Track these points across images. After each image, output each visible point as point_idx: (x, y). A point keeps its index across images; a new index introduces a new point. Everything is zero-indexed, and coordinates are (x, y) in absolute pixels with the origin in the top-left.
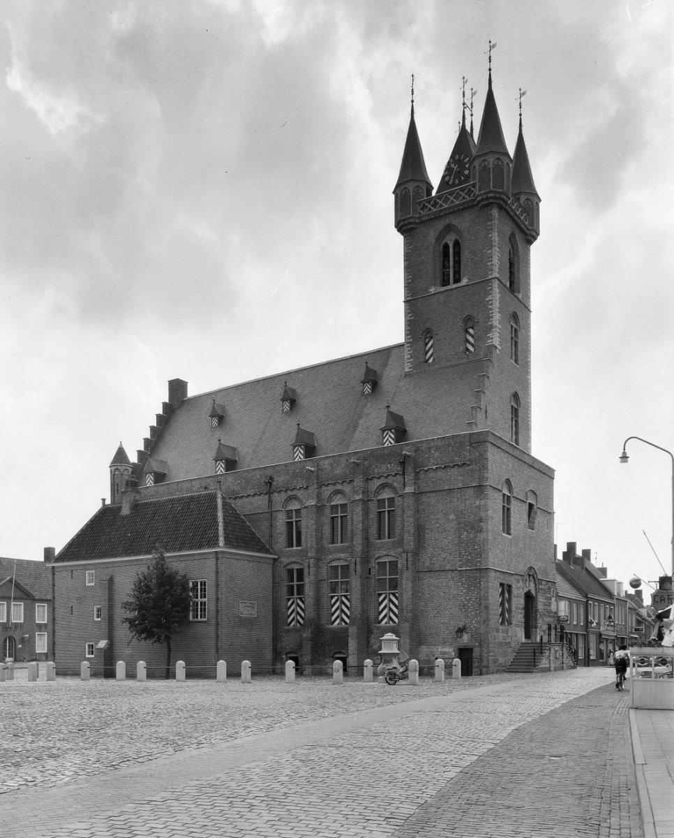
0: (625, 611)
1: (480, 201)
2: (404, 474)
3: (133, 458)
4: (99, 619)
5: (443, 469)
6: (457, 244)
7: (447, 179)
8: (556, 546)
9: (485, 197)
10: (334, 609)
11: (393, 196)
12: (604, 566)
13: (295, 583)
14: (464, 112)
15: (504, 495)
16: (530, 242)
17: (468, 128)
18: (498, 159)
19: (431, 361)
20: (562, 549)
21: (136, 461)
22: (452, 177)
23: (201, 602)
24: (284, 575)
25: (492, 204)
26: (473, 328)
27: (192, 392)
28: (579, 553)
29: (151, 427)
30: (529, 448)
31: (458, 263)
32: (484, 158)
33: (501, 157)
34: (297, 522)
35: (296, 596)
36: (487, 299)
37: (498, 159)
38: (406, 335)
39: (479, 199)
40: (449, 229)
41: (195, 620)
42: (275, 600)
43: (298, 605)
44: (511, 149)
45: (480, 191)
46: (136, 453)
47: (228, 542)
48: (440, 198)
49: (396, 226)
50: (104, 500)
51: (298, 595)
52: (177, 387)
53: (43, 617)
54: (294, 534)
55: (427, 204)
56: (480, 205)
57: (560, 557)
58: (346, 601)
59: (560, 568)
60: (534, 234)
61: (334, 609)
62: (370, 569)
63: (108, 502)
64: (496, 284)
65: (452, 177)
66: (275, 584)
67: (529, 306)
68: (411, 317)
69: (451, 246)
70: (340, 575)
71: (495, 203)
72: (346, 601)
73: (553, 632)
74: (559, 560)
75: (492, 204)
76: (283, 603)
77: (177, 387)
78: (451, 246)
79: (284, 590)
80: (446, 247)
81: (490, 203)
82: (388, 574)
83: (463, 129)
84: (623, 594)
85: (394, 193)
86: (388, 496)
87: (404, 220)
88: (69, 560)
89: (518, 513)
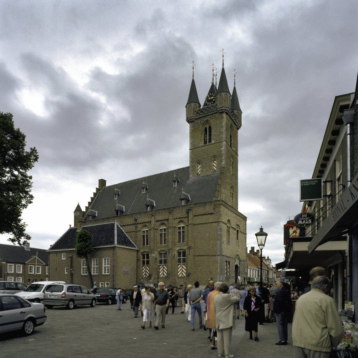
0: (272, 273)
1: (219, 111)
2: (188, 217)
3: (84, 209)
4: (67, 273)
6: (210, 128)
7: (207, 102)
8: (247, 248)
9: (221, 109)
11: (185, 109)
12: (265, 256)
13: (146, 260)
14: (213, 77)
15: (227, 226)
16: (238, 129)
17: (215, 84)
18: (195, 104)
19: (200, 173)
20: (249, 249)
21: (85, 211)
23: (96, 267)
26: (216, 160)
27: (108, 184)
28: (255, 251)
29: (88, 202)
30: (237, 208)
31: (210, 135)
32: (221, 94)
33: (227, 94)
34: (147, 235)
35: (146, 265)
37: (226, 94)
39: (219, 110)
41: (105, 274)
42: (138, 267)
44: (231, 92)
46: (90, 198)
47: (118, 243)
48: (204, 109)
49: (187, 120)
50: (70, 225)
51: (147, 264)
52: (102, 182)
53: (12, 270)
54: (146, 240)
55: (203, 110)
56: (219, 113)
57: (248, 252)
58: (184, 267)
59: (248, 255)
60: (239, 125)
63: (73, 226)
64: (224, 143)
66: (138, 260)
67: (238, 153)
68: (192, 156)
69: (208, 129)
72: (184, 267)
73: (246, 280)
74: (248, 253)
76: (141, 268)
77: (102, 182)
78: (208, 129)
79: (141, 263)
80: (206, 129)
83: (213, 84)
84: (271, 267)
85: (186, 107)
87: (190, 117)
88: (57, 249)
89: (233, 233)
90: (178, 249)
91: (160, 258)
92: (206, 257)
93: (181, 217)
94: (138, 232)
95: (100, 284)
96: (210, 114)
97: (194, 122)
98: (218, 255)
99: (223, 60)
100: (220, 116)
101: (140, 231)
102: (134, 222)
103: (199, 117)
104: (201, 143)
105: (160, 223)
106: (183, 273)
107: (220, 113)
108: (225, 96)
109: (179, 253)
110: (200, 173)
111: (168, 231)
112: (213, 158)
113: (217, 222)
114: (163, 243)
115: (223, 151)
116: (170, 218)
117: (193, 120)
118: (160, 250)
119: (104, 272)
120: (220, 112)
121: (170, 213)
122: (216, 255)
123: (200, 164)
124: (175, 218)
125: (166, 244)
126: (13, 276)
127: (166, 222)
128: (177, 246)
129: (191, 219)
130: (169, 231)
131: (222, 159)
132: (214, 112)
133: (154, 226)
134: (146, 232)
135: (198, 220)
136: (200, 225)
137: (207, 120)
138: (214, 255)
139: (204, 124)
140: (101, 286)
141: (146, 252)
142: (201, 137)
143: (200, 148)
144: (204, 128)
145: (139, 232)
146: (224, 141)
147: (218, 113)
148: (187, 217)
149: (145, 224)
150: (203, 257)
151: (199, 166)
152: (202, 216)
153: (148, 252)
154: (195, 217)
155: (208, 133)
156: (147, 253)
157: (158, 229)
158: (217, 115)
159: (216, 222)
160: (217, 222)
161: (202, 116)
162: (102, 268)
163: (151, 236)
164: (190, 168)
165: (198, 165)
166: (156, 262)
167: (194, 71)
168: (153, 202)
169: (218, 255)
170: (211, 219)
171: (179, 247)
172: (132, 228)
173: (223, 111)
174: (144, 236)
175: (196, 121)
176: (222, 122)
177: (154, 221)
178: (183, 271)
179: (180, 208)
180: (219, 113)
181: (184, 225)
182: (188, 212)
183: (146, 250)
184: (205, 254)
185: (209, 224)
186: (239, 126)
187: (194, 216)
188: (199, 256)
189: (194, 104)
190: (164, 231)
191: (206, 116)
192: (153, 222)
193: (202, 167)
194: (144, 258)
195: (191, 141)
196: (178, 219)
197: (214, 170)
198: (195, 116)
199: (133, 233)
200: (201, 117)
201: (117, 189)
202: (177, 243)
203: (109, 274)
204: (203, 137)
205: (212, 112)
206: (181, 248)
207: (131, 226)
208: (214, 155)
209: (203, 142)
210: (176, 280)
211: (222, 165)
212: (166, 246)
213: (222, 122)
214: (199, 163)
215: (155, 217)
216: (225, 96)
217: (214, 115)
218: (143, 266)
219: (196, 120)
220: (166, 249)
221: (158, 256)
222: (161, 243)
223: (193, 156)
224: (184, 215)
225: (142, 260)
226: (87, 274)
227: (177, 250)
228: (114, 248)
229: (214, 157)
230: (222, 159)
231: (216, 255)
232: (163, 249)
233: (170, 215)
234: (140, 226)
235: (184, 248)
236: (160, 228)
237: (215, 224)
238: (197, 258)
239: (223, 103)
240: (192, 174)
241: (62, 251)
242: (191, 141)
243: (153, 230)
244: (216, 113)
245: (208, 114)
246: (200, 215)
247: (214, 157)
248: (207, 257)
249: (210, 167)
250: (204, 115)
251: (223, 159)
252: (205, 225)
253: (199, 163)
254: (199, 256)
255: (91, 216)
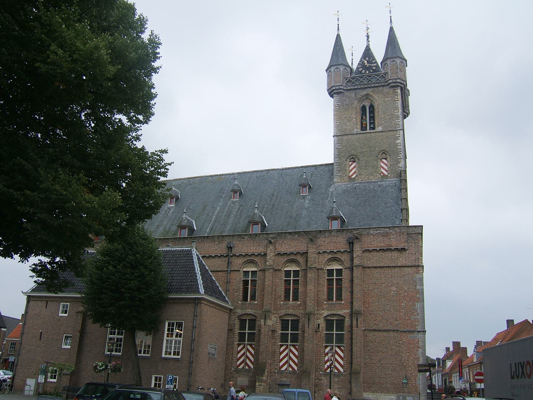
1: (391, 83)
5: (328, 253)
6: (372, 107)
9: (394, 81)
10: (239, 355)
18: (345, 69)
19: (353, 177)
22: (372, 65)
24: (237, 323)
25: (398, 86)
26: (386, 159)
31: (372, 118)
32: (394, 60)
33: (403, 61)
36: (396, 142)
38: (335, 158)
40: (367, 96)
41: (168, 356)
42: (229, 345)
43: (248, 350)
45: (390, 77)
61: (239, 355)
62: (319, 325)
65: (372, 65)
66: (230, 330)
68: (338, 146)
70: (244, 331)
71: (399, 86)
75: (398, 86)
76: (235, 349)
81: (398, 85)
82: (288, 332)
86: (336, 268)
90: (326, 313)
91: (282, 330)
92: (391, 334)
93: (335, 251)
94: (232, 272)
95: (51, 380)
96: (373, 85)
97: (342, 94)
98: (420, 332)
99: (391, 17)
100: (392, 91)
101: (239, 271)
102: (224, 252)
103: (352, 88)
104: (357, 128)
105: (286, 258)
106: (248, 361)
107: (392, 87)
108: (400, 63)
109: (329, 324)
110: (353, 177)
111: (306, 277)
112: (381, 154)
113: (415, 266)
114: (291, 300)
115: (400, 146)
116: (312, 251)
117: (342, 91)
118: (283, 312)
119: (166, 352)
120: (392, 85)
121: (311, 240)
122: (414, 332)
123: (354, 162)
124: (321, 251)
125: (299, 303)
126: (122, 353)
127: (300, 259)
128: (325, 307)
129: (358, 256)
130: (309, 275)
131: (399, 158)
132: (380, 85)
133: (272, 263)
134: (251, 272)
135: (375, 259)
136: (378, 269)
137: (367, 95)
138: (409, 331)
139: (360, 100)
140: (155, 384)
141: (250, 314)
142: (356, 118)
143: (354, 136)
144: (361, 106)
145: (236, 273)
146: (401, 130)
147: (388, 87)
148: (349, 252)
149: (250, 258)
150: (385, 334)
151: (351, 165)
152: (381, 253)
153: (255, 316)
154: (366, 254)
155: (368, 114)
156: (251, 317)
157: (280, 270)
158: (386, 90)
159: (412, 266)
160: (415, 266)
161: (359, 87)
162: (162, 343)
163: (266, 283)
164: (335, 167)
165: (350, 163)
166: (273, 337)
167: (339, 23)
168: (192, 222)
169: (418, 331)
170: (402, 259)
171: (328, 309)
172: (222, 264)
173: (398, 84)
174: (246, 283)
175: (348, 93)
176: (397, 101)
177: (272, 254)
178: (290, 358)
179: (333, 233)
180: (390, 86)
181: (255, 269)
182: (353, 243)
183: (249, 311)
184: (388, 328)
185: (397, 270)
186: (407, 113)
187: (363, 252)
188: (375, 330)
189: (401, 61)
190: (252, 275)
191: (366, 88)
192: (271, 255)
193: (359, 167)
194: (242, 327)
195: (336, 123)
196: (326, 254)
197: (382, 175)
198: (345, 85)
199: (220, 273)
200: (356, 89)
201: (175, 189)
202: (325, 302)
203: (179, 357)
204: (359, 118)
205: (377, 83)
206: (335, 312)
207: (217, 260)
208: (382, 149)
209: (359, 127)
210: (320, 380)
211: (399, 167)
212: (299, 305)
213: (397, 101)
214: (352, 160)
215: (275, 246)
216: (400, 63)
217: (381, 88)
218: (239, 345)
219: (345, 92)
220: (299, 312)
221: (279, 326)
222: (287, 297)
223: (339, 147)
224: (342, 248)
225: (237, 331)
226: (120, 354)
227: (325, 315)
228: (197, 301)
229: (353, 158)
230: (399, 158)
231: (414, 332)
232: (291, 311)
233: (309, 246)
234: (241, 261)
235: (341, 312)
236: (286, 269)
237: (409, 269)
238: (371, 336)
239: (398, 72)
240: (339, 176)
241: (61, 297)
242: (336, 123)
243: (271, 271)
244: (383, 86)
245: (369, 86)
246: (213, 257)
247: (353, 158)
248: (395, 334)
249: (376, 168)
250: (363, 87)
251: (401, 158)
252: (387, 271)
253: (352, 160)
254: (375, 330)
255: (187, 229)
